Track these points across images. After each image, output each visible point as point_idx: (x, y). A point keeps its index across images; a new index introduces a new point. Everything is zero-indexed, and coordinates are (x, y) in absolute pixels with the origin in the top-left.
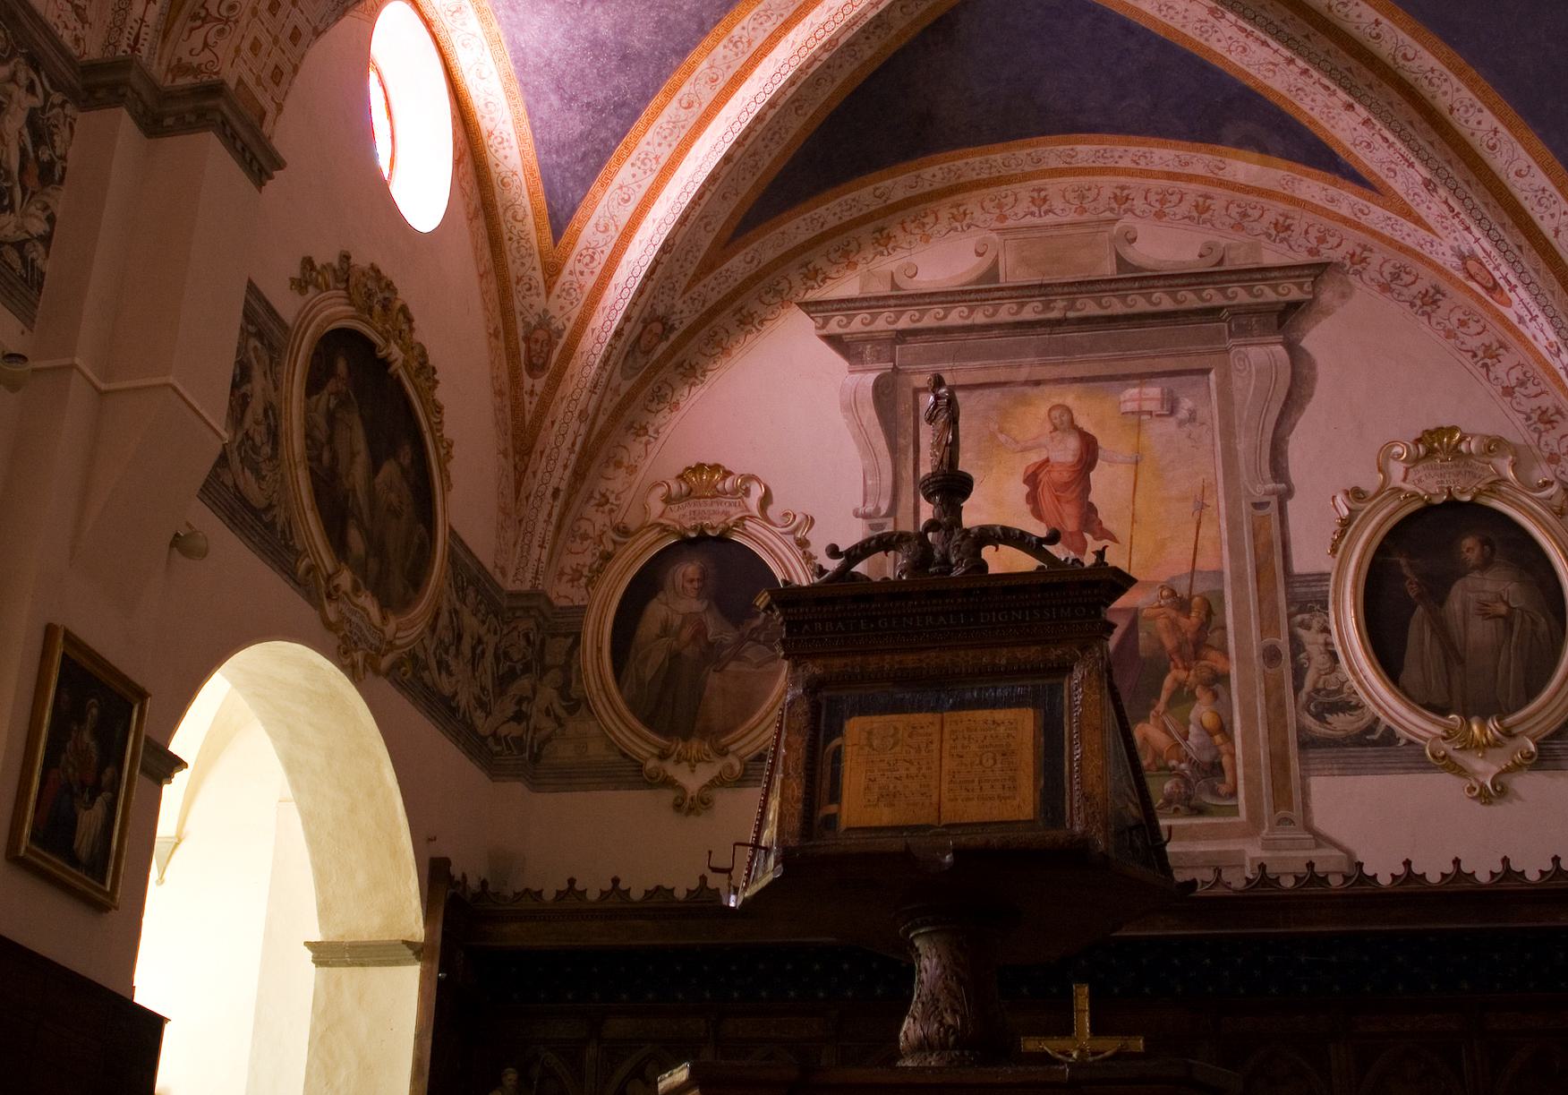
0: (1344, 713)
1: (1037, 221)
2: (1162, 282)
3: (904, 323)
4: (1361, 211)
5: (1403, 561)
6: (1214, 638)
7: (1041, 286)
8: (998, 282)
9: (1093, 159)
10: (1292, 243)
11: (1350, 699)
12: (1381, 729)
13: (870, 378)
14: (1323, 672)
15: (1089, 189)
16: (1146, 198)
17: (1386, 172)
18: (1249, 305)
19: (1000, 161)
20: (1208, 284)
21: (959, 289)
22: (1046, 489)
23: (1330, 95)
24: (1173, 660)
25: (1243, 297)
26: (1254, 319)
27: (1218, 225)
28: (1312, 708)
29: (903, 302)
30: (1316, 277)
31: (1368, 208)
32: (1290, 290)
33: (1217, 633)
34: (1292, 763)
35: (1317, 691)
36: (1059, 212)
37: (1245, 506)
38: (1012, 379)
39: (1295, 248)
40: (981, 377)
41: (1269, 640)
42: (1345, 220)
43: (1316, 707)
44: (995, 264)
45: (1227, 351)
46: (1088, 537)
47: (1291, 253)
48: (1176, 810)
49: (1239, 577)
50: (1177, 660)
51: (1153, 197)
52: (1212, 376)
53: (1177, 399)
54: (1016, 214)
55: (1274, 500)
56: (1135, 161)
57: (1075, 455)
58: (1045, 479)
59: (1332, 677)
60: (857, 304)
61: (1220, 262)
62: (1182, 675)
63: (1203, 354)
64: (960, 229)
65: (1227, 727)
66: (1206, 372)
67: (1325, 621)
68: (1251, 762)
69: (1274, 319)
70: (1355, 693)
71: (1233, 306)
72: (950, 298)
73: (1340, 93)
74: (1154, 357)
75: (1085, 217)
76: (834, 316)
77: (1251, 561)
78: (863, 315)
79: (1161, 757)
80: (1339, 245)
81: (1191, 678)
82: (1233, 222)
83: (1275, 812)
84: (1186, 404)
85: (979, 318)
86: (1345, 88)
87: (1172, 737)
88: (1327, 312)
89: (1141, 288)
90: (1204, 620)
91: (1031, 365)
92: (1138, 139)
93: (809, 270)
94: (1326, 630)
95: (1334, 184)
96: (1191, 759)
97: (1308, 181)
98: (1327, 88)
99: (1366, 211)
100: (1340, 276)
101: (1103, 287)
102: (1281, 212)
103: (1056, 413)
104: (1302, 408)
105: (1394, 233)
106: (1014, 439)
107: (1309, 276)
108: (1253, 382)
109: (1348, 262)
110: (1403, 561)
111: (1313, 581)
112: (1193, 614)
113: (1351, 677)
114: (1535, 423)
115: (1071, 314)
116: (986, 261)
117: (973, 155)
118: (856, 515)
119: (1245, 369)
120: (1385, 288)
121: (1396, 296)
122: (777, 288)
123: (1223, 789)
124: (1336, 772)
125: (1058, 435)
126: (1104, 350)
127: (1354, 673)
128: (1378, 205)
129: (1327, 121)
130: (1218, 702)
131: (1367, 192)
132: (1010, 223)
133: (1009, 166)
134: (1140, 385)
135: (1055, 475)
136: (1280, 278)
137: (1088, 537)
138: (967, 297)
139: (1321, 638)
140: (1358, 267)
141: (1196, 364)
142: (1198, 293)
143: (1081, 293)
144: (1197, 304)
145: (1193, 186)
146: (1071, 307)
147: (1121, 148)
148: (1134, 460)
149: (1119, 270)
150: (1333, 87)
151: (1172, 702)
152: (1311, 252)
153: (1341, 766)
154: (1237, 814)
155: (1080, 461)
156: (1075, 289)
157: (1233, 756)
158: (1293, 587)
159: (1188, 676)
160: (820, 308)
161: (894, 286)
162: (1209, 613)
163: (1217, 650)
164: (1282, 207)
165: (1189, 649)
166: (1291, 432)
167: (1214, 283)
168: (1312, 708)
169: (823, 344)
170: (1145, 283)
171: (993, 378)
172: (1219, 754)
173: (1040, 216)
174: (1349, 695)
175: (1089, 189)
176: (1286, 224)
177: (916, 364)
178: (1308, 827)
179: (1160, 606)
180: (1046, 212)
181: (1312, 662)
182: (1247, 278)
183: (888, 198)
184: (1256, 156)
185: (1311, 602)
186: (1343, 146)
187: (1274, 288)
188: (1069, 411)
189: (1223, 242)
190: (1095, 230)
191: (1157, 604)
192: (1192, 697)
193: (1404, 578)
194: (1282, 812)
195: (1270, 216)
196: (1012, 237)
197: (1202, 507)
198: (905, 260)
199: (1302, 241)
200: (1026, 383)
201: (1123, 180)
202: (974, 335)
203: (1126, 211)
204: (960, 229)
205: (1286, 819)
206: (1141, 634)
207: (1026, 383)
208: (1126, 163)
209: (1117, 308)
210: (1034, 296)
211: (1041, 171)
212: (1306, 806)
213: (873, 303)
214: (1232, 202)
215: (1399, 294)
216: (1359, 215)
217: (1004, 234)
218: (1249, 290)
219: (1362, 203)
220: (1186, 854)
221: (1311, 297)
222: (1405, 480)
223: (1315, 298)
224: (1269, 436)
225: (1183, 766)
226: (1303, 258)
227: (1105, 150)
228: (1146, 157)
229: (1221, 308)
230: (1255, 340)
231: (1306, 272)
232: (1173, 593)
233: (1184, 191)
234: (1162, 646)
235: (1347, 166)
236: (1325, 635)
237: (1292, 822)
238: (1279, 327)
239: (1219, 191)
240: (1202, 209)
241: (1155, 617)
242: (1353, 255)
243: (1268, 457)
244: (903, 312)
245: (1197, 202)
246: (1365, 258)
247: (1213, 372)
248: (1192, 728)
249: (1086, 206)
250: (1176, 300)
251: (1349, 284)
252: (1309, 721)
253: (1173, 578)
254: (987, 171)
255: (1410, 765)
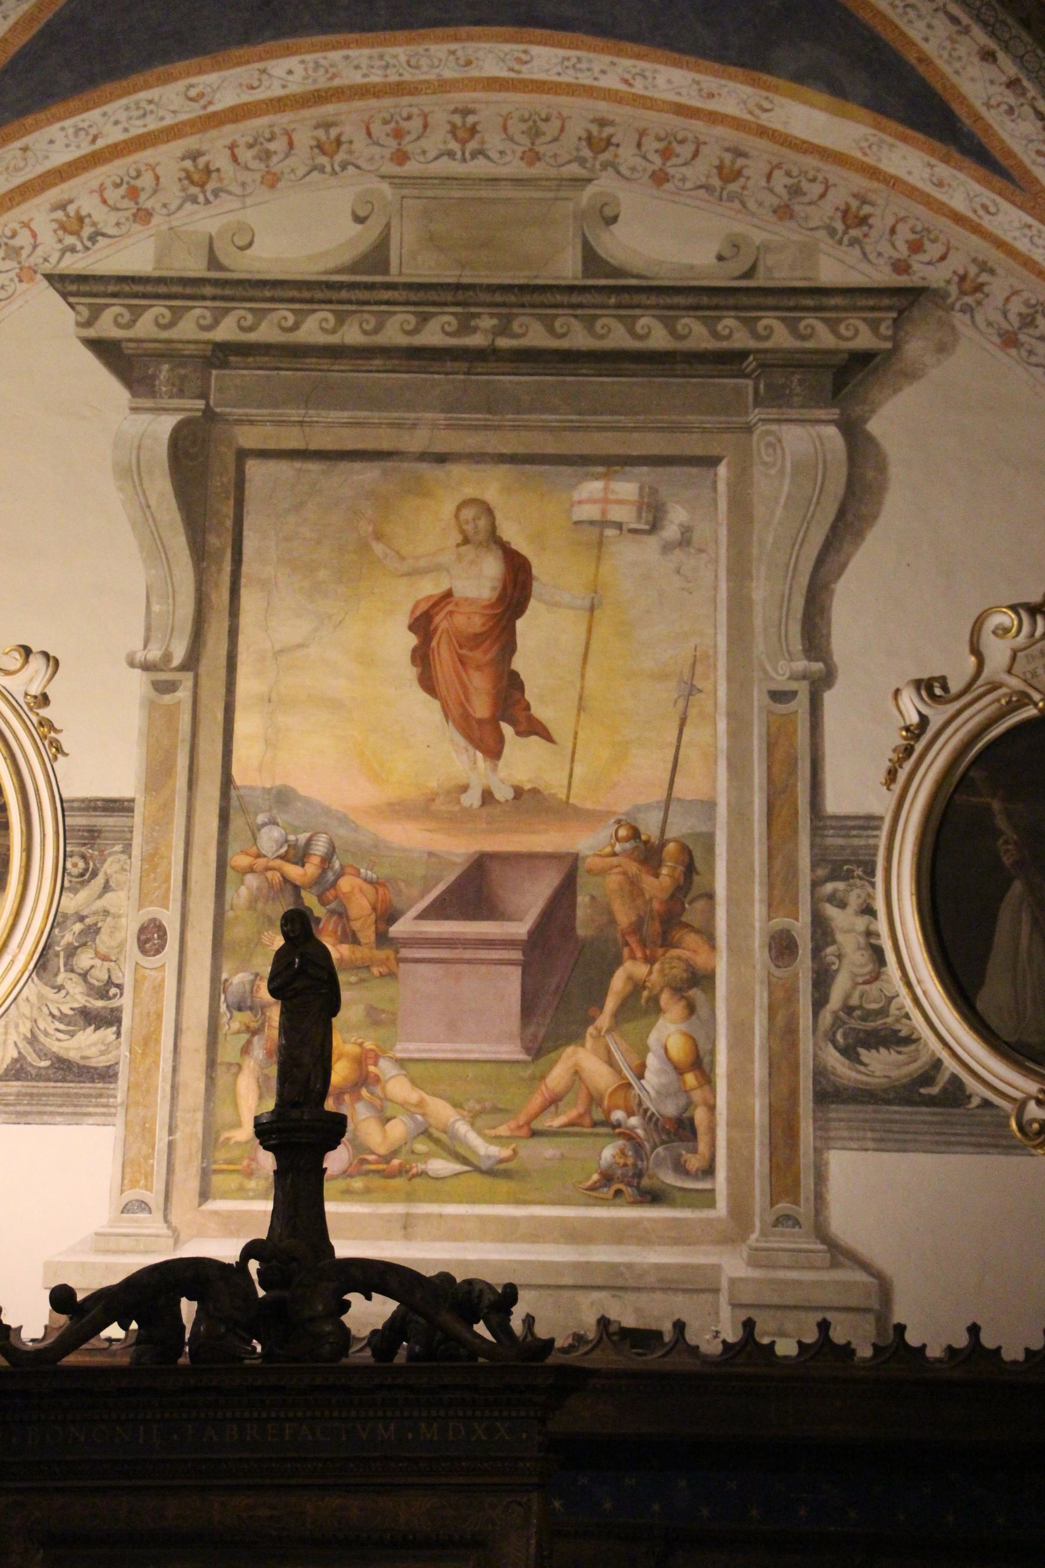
0: (888, 1048)
1: (455, 168)
2: (653, 300)
3: (226, 331)
4: (985, 207)
5: (996, 806)
6: (693, 913)
7: (458, 287)
8: (386, 271)
9: (559, 69)
10: (868, 249)
11: (898, 1027)
12: (942, 1079)
13: (167, 424)
14: (860, 980)
15: (547, 120)
16: (639, 145)
17: (1033, 155)
18: (789, 351)
19: (403, 58)
20: (727, 308)
21: (324, 278)
22: (444, 640)
23: (959, 33)
24: (627, 944)
25: (781, 338)
26: (796, 378)
27: (752, 205)
28: (839, 1037)
29: (228, 292)
30: (901, 312)
31: (996, 204)
32: (857, 332)
33: (700, 905)
34: (803, 1125)
35: (849, 1009)
36: (494, 155)
37: (758, 698)
38: (402, 447)
39: (872, 256)
40: (351, 440)
41: (780, 922)
42: (958, 218)
43: (845, 1036)
44: (383, 244)
45: (749, 429)
46: (507, 729)
47: (865, 267)
48: (618, 1193)
49: (739, 814)
50: (634, 945)
51: (651, 145)
52: (722, 470)
53: (663, 504)
54: (424, 152)
55: (803, 688)
56: (626, 81)
57: (494, 589)
58: (444, 625)
59: (873, 989)
60: (149, 289)
61: (749, 274)
62: (640, 970)
63: (710, 431)
64: (328, 169)
65: (706, 1060)
66: (713, 462)
67: (869, 896)
68: (739, 1121)
69: (828, 380)
70: (907, 1016)
71: (765, 351)
72: (306, 295)
73: (977, 31)
74: (635, 429)
75: (538, 170)
76: (107, 306)
77: (761, 789)
78: (159, 310)
79: (600, 1104)
80: (943, 258)
81: (655, 977)
82: (776, 202)
83: (772, 1205)
84: (677, 516)
85: (352, 335)
86: (985, 24)
87: (619, 1072)
88: (912, 375)
89: (619, 306)
90: (682, 880)
91: (434, 426)
92: (636, 48)
93: (68, 216)
94: (869, 911)
95: (946, 160)
96: (646, 1111)
97: (903, 148)
98: (954, 20)
99: (992, 209)
100: (940, 313)
101: (559, 298)
102: (856, 190)
103: (468, 513)
104: (859, 536)
105: (1034, 249)
106: (398, 553)
107: (889, 309)
108: (786, 488)
109: (953, 290)
110: (996, 806)
111: (854, 828)
112: (664, 871)
113: (903, 991)
114: (722, 189)
115: (503, 343)
116: (372, 232)
117: (360, 44)
118: (132, 664)
119: (774, 464)
120: (1009, 340)
121: (1024, 354)
122: (11, 242)
123: (694, 1163)
124: (870, 1144)
125: (467, 550)
126: (554, 411)
127: (909, 985)
128: (1014, 203)
129: (949, 63)
130: (694, 1018)
131: (997, 181)
132: (412, 167)
133: (417, 67)
134: (605, 476)
135: (460, 620)
136: (845, 309)
137: (507, 729)
138: (334, 295)
139: (861, 923)
140: (969, 300)
141: (693, 445)
142: (710, 324)
143: (523, 306)
144: (709, 344)
145: (720, 130)
146: (504, 330)
147: (607, 59)
148: (587, 603)
149: (586, 272)
150: (965, 19)
151: (622, 1014)
152: (901, 267)
153: (877, 1135)
154: (712, 1204)
155: (501, 599)
156: (512, 299)
157: (712, 1108)
158: (824, 836)
159: (650, 973)
160: (85, 288)
161: (214, 262)
162: (690, 869)
163: (697, 931)
164: (859, 182)
165: (654, 928)
166: (839, 575)
167: (736, 308)
168: (839, 1037)
169: (89, 359)
170: (626, 298)
171: (369, 444)
172: (690, 1104)
173: (464, 160)
174: (898, 1020)
175: (547, 120)
176: (862, 213)
177: (245, 406)
178: (821, 1232)
179: (614, 854)
180: (474, 155)
181: (846, 961)
182: (792, 303)
183: (210, 103)
184: (824, 98)
185: (847, 862)
186: (970, 106)
187: (832, 325)
188: (489, 511)
189: (758, 237)
190: (552, 195)
191: (608, 850)
192: (655, 1008)
193: (997, 833)
194: (783, 1206)
195: (837, 197)
196: (416, 192)
197: (692, 690)
198: (231, 217)
199: (885, 247)
200: (423, 457)
201: (604, 108)
202: (344, 365)
203: (604, 166)
204: (328, 169)
205: (788, 1217)
206: (580, 899)
207: (423, 457)
208: (611, 82)
209: (580, 339)
210: (445, 304)
211: (471, 79)
212: (819, 1198)
213: (176, 289)
214: (779, 166)
215: (1030, 352)
216: (981, 212)
217: (401, 186)
218: (792, 325)
219: (987, 196)
220: (630, 1266)
221: (888, 345)
222: (1009, 671)
223: (897, 348)
224: (804, 580)
225: (634, 1121)
226: (883, 276)
227: (579, 60)
228: (645, 77)
229: (742, 355)
230: (794, 414)
231: (886, 302)
232: (635, 834)
233: (702, 138)
234: (613, 921)
235: (971, 136)
236: (867, 918)
237: (797, 1223)
238: (837, 390)
239: (762, 143)
240: (729, 175)
241: (603, 872)
242: (963, 278)
243: (799, 615)
244: (228, 311)
245: (722, 160)
246: (982, 285)
247: (724, 462)
248: (652, 1061)
249: (541, 149)
250: (673, 333)
251: (953, 328)
252: (834, 1059)
253: (638, 809)
254: (380, 72)
255: (983, 1140)
